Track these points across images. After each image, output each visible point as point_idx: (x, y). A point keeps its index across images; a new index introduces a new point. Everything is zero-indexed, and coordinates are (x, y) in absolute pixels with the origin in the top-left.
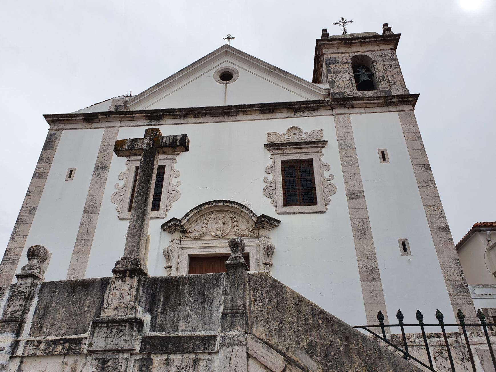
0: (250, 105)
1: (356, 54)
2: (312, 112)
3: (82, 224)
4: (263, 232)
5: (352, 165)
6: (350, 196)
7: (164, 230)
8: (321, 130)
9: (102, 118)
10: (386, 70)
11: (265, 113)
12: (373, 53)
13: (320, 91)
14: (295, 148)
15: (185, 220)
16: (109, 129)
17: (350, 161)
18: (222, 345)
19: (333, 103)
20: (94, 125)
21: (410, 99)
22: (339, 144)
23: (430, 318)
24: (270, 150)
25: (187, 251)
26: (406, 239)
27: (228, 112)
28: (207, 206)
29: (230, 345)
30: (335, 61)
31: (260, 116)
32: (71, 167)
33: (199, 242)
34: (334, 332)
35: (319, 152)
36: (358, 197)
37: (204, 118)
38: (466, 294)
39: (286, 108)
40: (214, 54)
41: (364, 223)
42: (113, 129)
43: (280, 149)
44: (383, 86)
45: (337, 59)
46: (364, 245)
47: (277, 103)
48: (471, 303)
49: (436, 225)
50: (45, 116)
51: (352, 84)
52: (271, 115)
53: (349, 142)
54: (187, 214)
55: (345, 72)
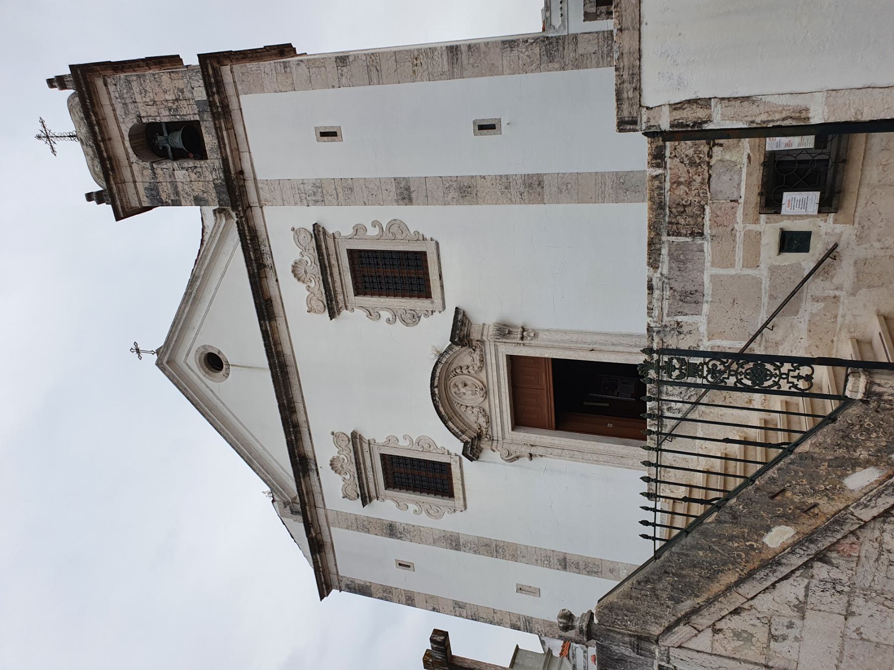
0: (264, 337)
1: (130, 150)
2: (260, 240)
3: (475, 552)
4: (475, 336)
5: (351, 189)
6: (406, 201)
7: (478, 458)
8: (293, 229)
9: (315, 531)
10: (155, 102)
11: (273, 313)
12: (121, 120)
13: (219, 227)
14: (331, 274)
15: (464, 436)
16: (330, 521)
17: (346, 191)
18: (668, 662)
19: (240, 209)
20: (326, 539)
21: (211, 72)
22: (315, 205)
23: (649, 516)
24: (339, 312)
25: (507, 433)
26: (474, 122)
27: (280, 368)
28: (441, 409)
29: (668, 657)
30: (152, 190)
31: (280, 321)
32: (394, 564)
33: (494, 417)
34: (660, 579)
35: (334, 238)
36: (408, 189)
37: (295, 399)
38: (560, 42)
39: (260, 282)
40: (178, 381)
41: (451, 186)
42: (330, 517)
43: (336, 297)
44: (189, 112)
45: (147, 185)
46: (486, 191)
47: (253, 294)
48: (575, 37)
49: (446, 68)
50: (322, 598)
51: (196, 167)
52: (274, 303)
53: (308, 188)
54: (455, 434)
55: (172, 175)
